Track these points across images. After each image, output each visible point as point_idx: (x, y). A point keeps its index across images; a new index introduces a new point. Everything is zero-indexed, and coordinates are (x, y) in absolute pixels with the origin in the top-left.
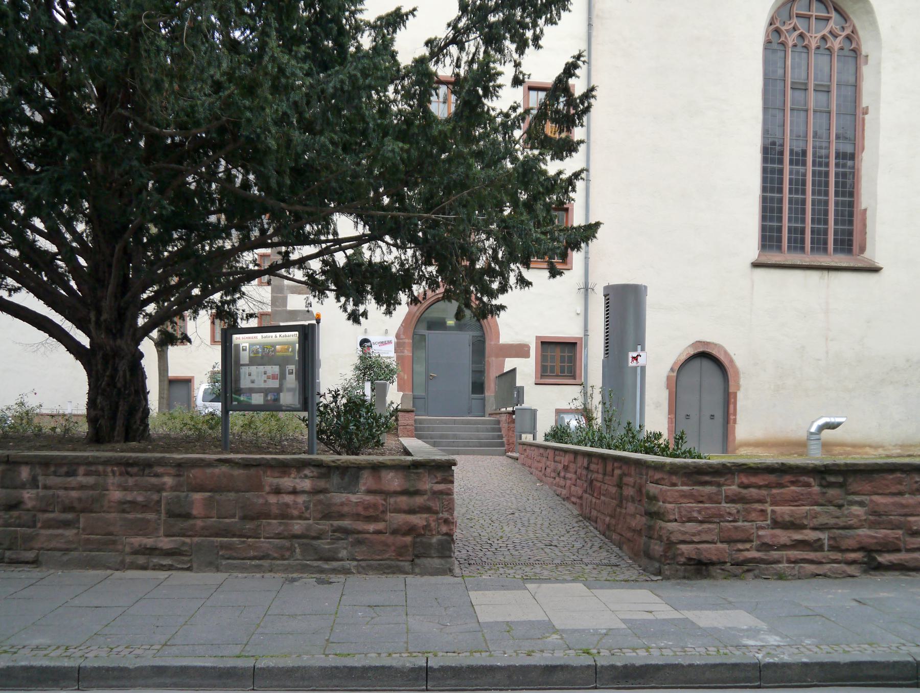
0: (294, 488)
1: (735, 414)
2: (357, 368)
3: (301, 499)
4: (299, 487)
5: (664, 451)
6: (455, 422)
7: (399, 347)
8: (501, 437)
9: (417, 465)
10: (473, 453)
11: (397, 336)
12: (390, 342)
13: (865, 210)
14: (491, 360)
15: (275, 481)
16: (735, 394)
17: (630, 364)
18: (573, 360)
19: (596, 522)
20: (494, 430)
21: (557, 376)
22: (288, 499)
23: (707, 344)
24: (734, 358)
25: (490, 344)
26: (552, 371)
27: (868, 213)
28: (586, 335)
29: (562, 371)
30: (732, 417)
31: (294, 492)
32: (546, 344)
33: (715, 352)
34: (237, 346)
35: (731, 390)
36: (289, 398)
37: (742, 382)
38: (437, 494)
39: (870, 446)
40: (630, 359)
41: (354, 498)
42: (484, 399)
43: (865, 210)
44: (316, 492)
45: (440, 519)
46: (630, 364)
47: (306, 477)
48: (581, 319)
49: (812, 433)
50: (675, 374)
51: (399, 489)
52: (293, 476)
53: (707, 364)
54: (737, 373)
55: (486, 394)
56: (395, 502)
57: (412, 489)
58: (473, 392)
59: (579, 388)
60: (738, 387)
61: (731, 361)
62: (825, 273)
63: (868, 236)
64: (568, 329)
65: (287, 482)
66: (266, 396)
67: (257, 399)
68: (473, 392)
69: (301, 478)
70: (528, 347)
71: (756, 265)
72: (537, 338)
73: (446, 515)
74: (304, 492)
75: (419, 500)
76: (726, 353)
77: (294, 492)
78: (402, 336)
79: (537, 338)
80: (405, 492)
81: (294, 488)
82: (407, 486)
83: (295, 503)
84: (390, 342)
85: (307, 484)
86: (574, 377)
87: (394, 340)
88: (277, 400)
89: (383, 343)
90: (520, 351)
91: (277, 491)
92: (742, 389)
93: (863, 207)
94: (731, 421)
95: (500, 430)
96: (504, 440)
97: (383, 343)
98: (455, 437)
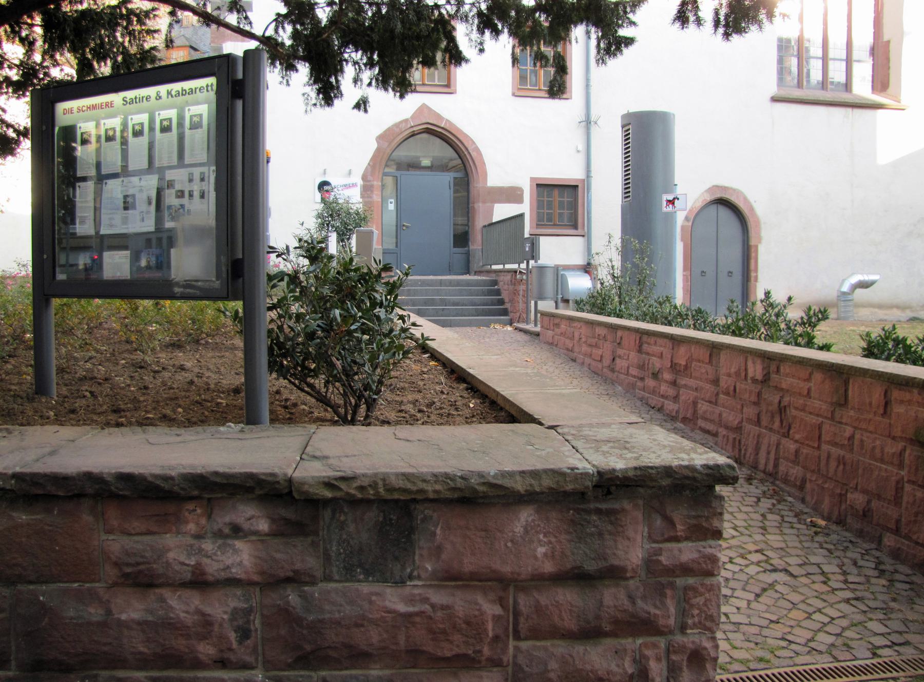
0: (198, 570)
1: (756, 270)
2: (319, 216)
3: (220, 607)
4: (212, 568)
5: (677, 318)
6: (441, 283)
7: (366, 190)
8: (501, 302)
9: (609, 485)
10: (469, 324)
11: (364, 178)
12: (354, 185)
13: (888, 42)
14: (480, 207)
15: (139, 544)
16: (756, 247)
17: (664, 210)
18: (574, 206)
19: (802, 488)
20: (490, 293)
21: (554, 225)
22: (182, 605)
23: (725, 189)
24: (755, 206)
25: (476, 186)
26: (549, 220)
27: (891, 45)
28: (588, 176)
29: (549, 220)
30: (753, 274)
31: (199, 582)
32: (544, 188)
33: (733, 199)
34: (69, 132)
35: (753, 242)
36: (191, 262)
37: (763, 234)
38: (659, 576)
39: (898, 307)
40: (665, 203)
41: (394, 600)
42: (468, 254)
43: (888, 42)
44: (273, 582)
45: (682, 649)
46: (664, 210)
47: (237, 531)
48: (581, 158)
49: (844, 293)
50: (690, 224)
51: (548, 567)
52: (191, 527)
53: (724, 212)
54: (758, 222)
55: (471, 247)
56: (539, 609)
57: (591, 566)
58: (454, 247)
59: (579, 240)
60: (759, 239)
61: (752, 209)
62: (849, 110)
63: (892, 72)
64: (570, 172)
65: (176, 548)
66: (135, 257)
67: (117, 265)
68: (454, 247)
69: (219, 534)
70: (521, 190)
71: (775, 100)
72: (532, 179)
73: (693, 638)
74: (233, 582)
75: (612, 598)
76: (745, 199)
77: (199, 582)
78: (370, 178)
79: (532, 179)
80: (578, 577)
81: (198, 570)
82: (580, 556)
83: (207, 622)
84: (354, 185)
85: (242, 558)
86: (575, 227)
87: (360, 182)
88: (163, 263)
89: (347, 186)
90: (512, 195)
91: (142, 579)
92: (763, 241)
93: (885, 39)
94: (752, 279)
95: (498, 292)
96: (507, 306)
97: (347, 186)
98: (444, 302)
